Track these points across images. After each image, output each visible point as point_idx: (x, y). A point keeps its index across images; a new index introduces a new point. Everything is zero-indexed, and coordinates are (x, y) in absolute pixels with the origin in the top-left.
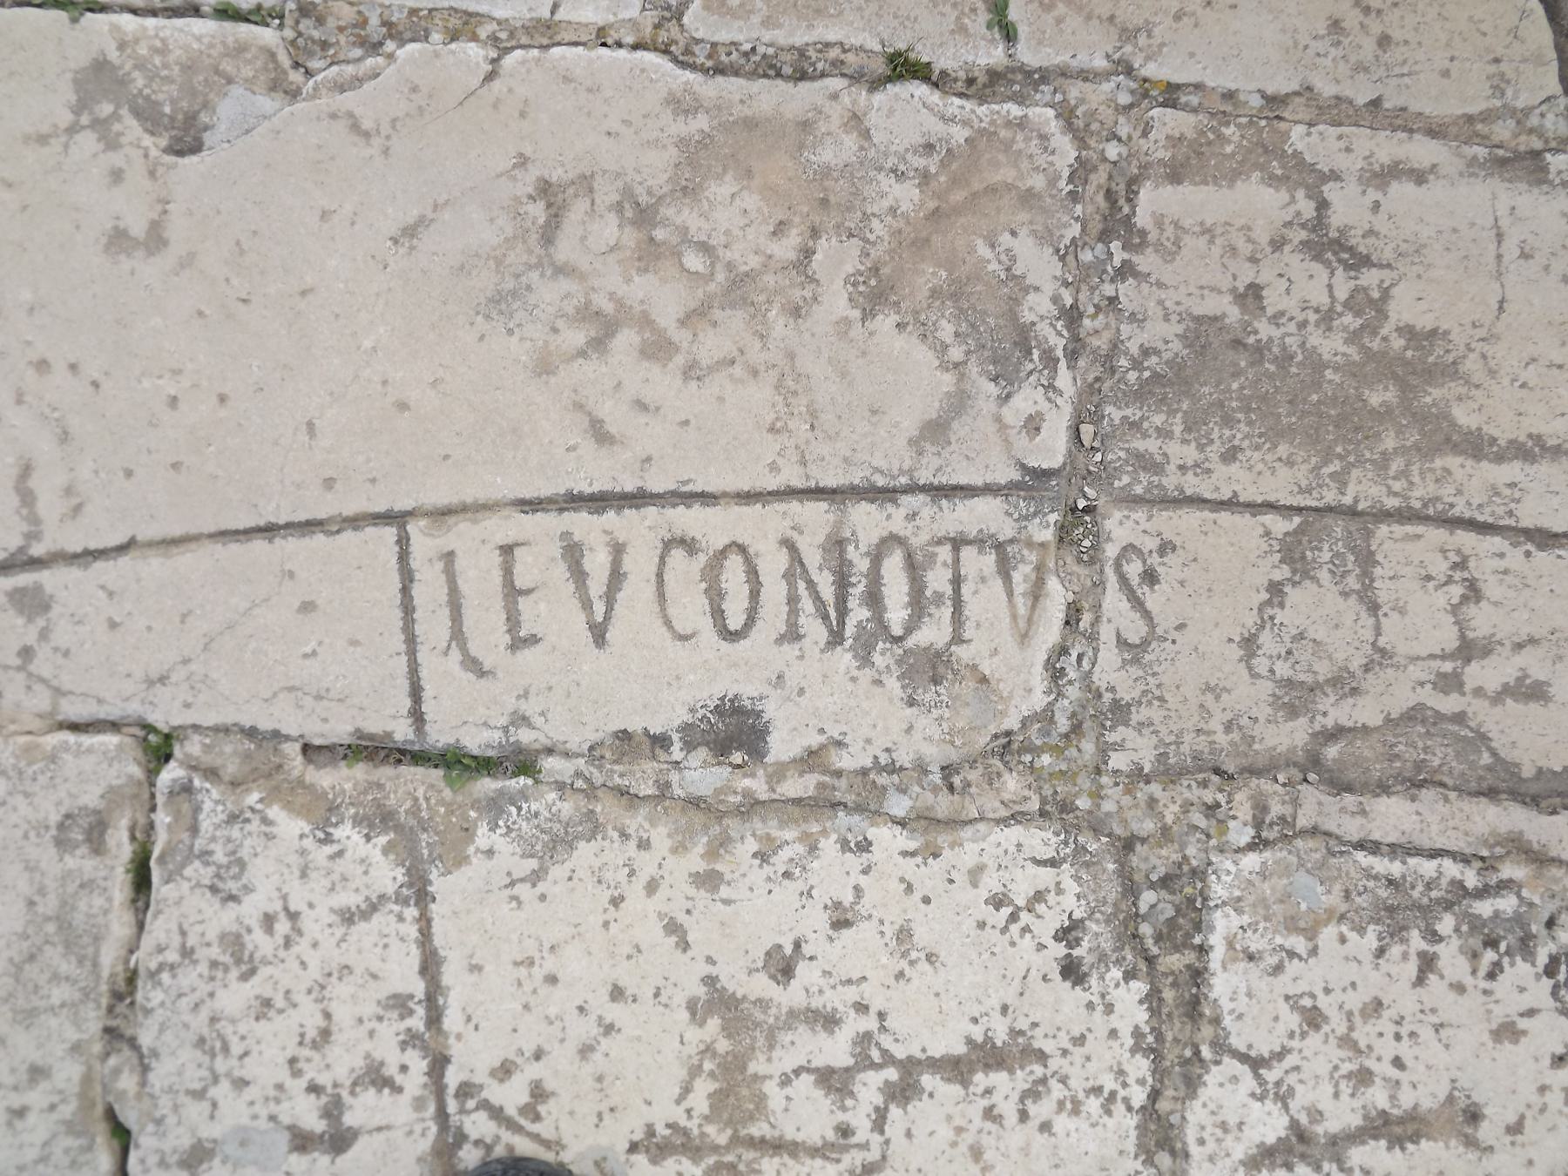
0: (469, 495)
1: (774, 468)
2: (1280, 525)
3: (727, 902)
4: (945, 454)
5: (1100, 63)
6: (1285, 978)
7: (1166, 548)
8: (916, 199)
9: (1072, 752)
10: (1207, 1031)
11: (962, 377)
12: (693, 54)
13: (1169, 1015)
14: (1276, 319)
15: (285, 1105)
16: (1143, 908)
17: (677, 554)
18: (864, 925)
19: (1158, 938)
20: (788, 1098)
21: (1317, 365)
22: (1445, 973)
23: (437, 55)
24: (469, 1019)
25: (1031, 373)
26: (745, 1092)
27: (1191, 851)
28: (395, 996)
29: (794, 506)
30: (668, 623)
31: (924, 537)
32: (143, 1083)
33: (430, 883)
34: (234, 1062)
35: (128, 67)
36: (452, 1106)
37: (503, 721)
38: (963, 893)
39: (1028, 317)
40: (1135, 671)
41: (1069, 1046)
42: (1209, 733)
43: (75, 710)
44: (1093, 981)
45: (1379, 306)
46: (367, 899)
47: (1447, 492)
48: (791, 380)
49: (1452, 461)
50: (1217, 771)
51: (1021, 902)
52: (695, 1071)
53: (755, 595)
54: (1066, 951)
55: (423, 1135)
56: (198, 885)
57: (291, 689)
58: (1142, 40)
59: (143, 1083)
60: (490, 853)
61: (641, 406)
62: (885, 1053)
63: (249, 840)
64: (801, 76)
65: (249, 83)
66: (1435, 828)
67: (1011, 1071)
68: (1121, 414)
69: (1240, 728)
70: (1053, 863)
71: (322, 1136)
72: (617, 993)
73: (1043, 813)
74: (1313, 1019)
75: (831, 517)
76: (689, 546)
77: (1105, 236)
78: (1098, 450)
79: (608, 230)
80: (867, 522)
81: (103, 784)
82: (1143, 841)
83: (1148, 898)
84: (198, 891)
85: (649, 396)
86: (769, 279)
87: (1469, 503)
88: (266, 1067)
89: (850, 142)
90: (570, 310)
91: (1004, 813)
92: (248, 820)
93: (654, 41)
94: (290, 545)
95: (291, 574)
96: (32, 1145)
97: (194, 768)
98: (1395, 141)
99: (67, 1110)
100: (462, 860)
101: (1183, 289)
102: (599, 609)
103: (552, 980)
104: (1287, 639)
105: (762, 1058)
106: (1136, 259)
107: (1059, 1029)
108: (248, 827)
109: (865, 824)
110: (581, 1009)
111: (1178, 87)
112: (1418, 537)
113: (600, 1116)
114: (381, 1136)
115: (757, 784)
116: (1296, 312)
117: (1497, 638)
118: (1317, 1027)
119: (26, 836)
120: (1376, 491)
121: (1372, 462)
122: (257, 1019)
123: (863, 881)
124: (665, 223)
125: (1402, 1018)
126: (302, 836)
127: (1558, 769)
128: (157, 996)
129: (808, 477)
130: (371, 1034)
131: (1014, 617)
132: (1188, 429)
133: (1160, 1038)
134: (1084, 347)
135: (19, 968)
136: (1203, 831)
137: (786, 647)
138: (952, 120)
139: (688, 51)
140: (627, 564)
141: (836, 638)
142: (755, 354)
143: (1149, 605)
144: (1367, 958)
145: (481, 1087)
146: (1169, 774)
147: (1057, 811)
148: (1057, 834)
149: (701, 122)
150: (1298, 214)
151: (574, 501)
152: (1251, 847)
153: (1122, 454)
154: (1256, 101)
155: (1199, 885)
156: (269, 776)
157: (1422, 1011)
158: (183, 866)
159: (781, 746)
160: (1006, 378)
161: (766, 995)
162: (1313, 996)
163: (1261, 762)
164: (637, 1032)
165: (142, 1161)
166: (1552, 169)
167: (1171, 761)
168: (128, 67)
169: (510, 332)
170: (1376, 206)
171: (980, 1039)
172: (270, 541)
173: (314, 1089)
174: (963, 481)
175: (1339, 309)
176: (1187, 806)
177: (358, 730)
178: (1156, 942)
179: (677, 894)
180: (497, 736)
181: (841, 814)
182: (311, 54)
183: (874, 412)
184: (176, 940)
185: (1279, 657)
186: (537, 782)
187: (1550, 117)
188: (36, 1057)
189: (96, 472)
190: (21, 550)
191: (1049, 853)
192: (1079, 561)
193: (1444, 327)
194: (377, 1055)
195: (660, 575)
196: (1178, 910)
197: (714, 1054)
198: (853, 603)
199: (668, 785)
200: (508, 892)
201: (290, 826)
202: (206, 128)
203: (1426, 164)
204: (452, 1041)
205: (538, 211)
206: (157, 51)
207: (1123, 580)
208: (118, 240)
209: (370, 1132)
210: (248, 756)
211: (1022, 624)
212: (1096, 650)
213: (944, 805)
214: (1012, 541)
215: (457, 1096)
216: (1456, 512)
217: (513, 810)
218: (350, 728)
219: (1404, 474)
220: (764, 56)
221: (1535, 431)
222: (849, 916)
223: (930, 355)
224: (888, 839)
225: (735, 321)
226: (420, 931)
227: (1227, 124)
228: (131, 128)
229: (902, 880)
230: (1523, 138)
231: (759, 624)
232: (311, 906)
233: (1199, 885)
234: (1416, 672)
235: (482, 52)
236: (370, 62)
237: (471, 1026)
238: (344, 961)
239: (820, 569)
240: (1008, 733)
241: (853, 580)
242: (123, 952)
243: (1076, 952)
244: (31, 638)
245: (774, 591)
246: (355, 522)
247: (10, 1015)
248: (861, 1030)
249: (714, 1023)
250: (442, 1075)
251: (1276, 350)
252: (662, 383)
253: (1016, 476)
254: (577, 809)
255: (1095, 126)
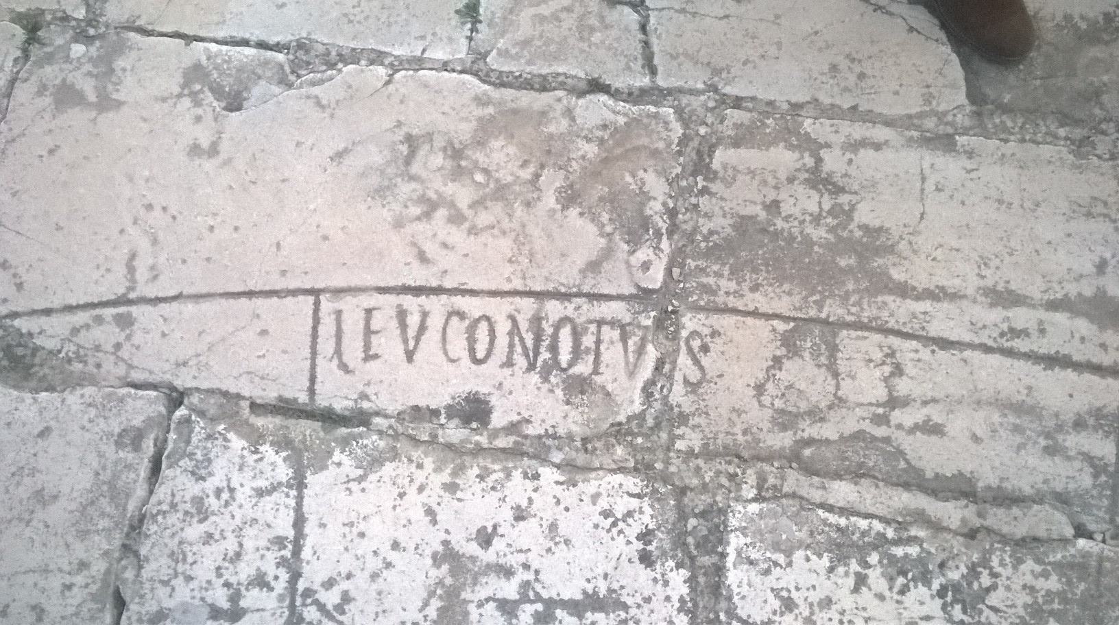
0: (355, 282)
1: (509, 280)
2: (781, 326)
3: (459, 500)
4: (598, 278)
5: (700, 86)
6: (771, 578)
7: (715, 334)
8: (596, 152)
9: (655, 438)
10: (723, 604)
11: (610, 240)
12: (489, 76)
13: (702, 592)
14: (787, 219)
15: (210, 592)
16: (690, 528)
17: (455, 319)
18: (533, 520)
19: (697, 546)
20: (481, 615)
21: (808, 242)
22: (872, 587)
23: (362, 71)
24: (315, 553)
25: (647, 240)
26: (458, 609)
27: (719, 498)
28: (278, 537)
29: (517, 299)
30: (446, 353)
31: (583, 319)
32: (138, 575)
33: (306, 478)
34: (188, 567)
35: (211, 68)
36: (299, 601)
37: (355, 396)
38: (587, 507)
39: (648, 212)
40: (692, 397)
41: (642, 603)
42: (733, 434)
43: (137, 376)
44: (658, 566)
45: (849, 214)
46: (272, 484)
47: (885, 314)
48: (521, 238)
49: (889, 299)
50: (738, 457)
51: (619, 516)
52: (432, 594)
53: (492, 342)
54: (642, 547)
55: (281, 616)
56: (185, 470)
57: (249, 373)
58: (724, 75)
59: (138, 575)
60: (339, 464)
61: (445, 245)
62: (537, 594)
63: (215, 449)
64: (544, 89)
65: (269, 82)
66: (868, 501)
67: (607, 614)
68: (695, 263)
69: (752, 434)
70: (639, 496)
71: (227, 611)
72: (396, 546)
73: (636, 469)
74: (789, 605)
75: (535, 306)
76: (461, 315)
77: (694, 174)
78: (681, 282)
79: (438, 160)
80: (554, 309)
81: (146, 415)
82: (692, 490)
83: (692, 522)
84: (185, 474)
85: (450, 240)
86: (517, 188)
87: (897, 322)
88: (204, 571)
89: (564, 123)
90: (415, 197)
91: (614, 466)
92: (217, 439)
93: (471, 69)
94: (259, 302)
95: (258, 316)
96: (71, 605)
97: (194, 410)
98: (864, 127)
99: (94, 588)
100: (324, 467)
101: (735, 202)
102: (411, 344)
103: (362, 535)
104: (782, 387)
105: (469, 590)
106: (710, 185)
107: (636, 592)
108: (216, 442)
109: (537, 465)
110: (375, 552)
111: (742, 98)
112: (866, 338)
113: (377, 614)
114: (257, 615)
115: (483, 440)
116: (798, 215)
117: (913, 397)
118: (791, 611)
119: (101, 439)
120: (840, 311)
121: (839, 296)
122: (204, 544)
123: (534, 495)
124: (467, 158)
125: (844, 611)
126: (243, 449)
127: (949, 475)
128: (154, 528)
129: (526, 286)
130: (262, 557)
131: (627, 363)
132: (732, 273)
133: (695, 605)
134: (678, 229)
135: (85, 508)
136: (726, 488)
137: (505, 370)
138: (618, 113)
139: (487, 75)
140: (429, 322)
141: (531, 367)
142: (506, 224)
143: (703, 363)
144: (823, 572)
145: (316, 592)
146: (708, 454)
147: (642, 469)
148: (642, 481)
149: (490, 110)
150: (805, 165)
151: (405, 290)
152: (755, 500)
153: (694, 284)
154: (785, 106)
155: (723, 518)
156: (231, 417)
157: (857, 608)
158: (179, 460)
159: (498, 420)
160: (634, 242)
161: (475, 554)
162: (789, 591)
163: (763, 454)
164: (403, 569)
165: (129, 618)
166: (959, 143)
167: (711, 448)
168: (211, 68)
169: (384, 206)
170: (850, 161)
171: (591, 592)
172: (250, 299)
173: (227, 585)
174: (606, 292)
175: (824, 214)
176: (718, 473)
177: (280, 396)
178: (696, 548)
179: (434, 493)
180: (351, 404)
181: (525, 459)
182: (301, 67)
183: (563, 255)
184: (169, 498)
185: (777, 397)
186: (368, 429)
187: (959, 116)
188: (83, 556)
189: (168, 260)
190: (124, 295)
191: (637, 491)
192: (667, 338)
193: (887, 225)
194: (263, 569)
195: (444, 329)
196: (709, 531)
197: (443, 585)
198: (542, 350)
199: (436, 436)
200: (345, 486)
201: (237, 443)
202: (245, 99)
203: (882, 140)
204: (304, 564)
205: (404, 149)
206: (226, 61)
207: (690, 350)
208: (195, 150)
209: (252, 611)
210: (221, 406)
211: (631, 367)
212: (672, 385)
213: (581, 458)
214: (629, 324)
215: (302, 596)
216: (890, 325)
217: (354, 443)
218: (276, 395)
219: (858, 303)
220: (526, 79)
221: (940, 284)
222: (524, 514)
223: (595, 229)
224: (549, 475)
225: (498, 208)
226: (297, 503)
227: (768, 118)
228: (209, 97)
229: (555, 497)
230: (941, 127)
231: (493, 357)
232: (242, 485)
233: (723, 518)
234: (859, 412)
235: (385, 71)
236: (329, 72)
237: (315, 557)
238: (254, 516)
239: (527, 331)
240: (620, 424)
241: (544, 338)
242: (140, 504)
243: (649, 548)
244: (122, 338)
245: (502, 341)
246: (295, 293)
247: (74, 533)
248: (525, 579)
249: (445, 568)
250: (296, 583)
251: (785, 234)
252: (456, 236)
253: (634, 291)
254: (388, 444)
255: (694, 118)
